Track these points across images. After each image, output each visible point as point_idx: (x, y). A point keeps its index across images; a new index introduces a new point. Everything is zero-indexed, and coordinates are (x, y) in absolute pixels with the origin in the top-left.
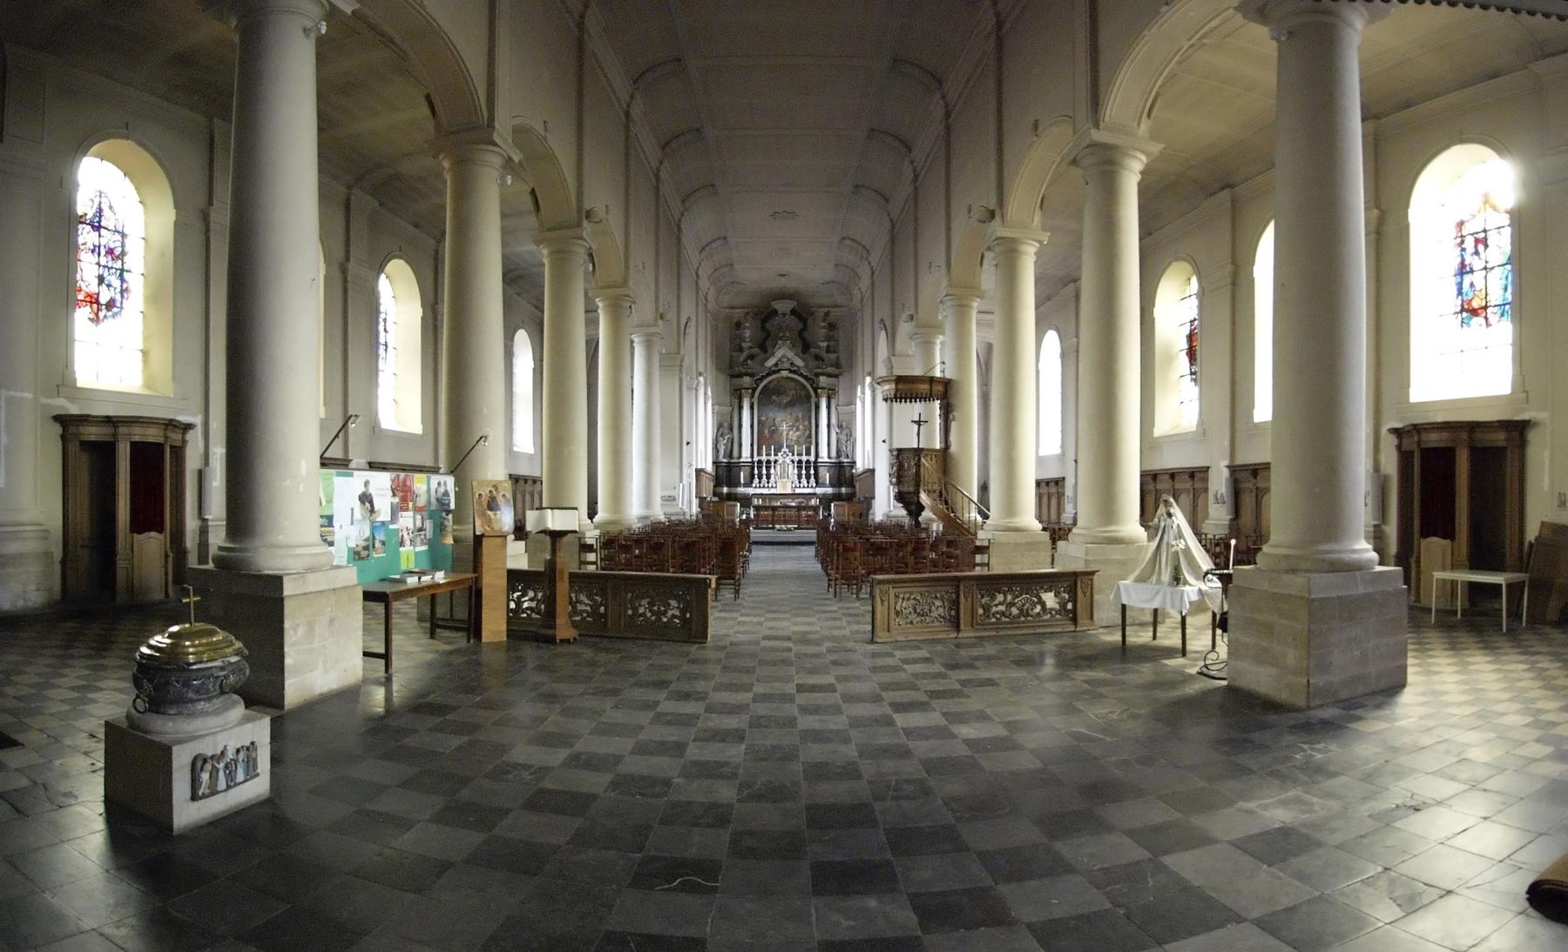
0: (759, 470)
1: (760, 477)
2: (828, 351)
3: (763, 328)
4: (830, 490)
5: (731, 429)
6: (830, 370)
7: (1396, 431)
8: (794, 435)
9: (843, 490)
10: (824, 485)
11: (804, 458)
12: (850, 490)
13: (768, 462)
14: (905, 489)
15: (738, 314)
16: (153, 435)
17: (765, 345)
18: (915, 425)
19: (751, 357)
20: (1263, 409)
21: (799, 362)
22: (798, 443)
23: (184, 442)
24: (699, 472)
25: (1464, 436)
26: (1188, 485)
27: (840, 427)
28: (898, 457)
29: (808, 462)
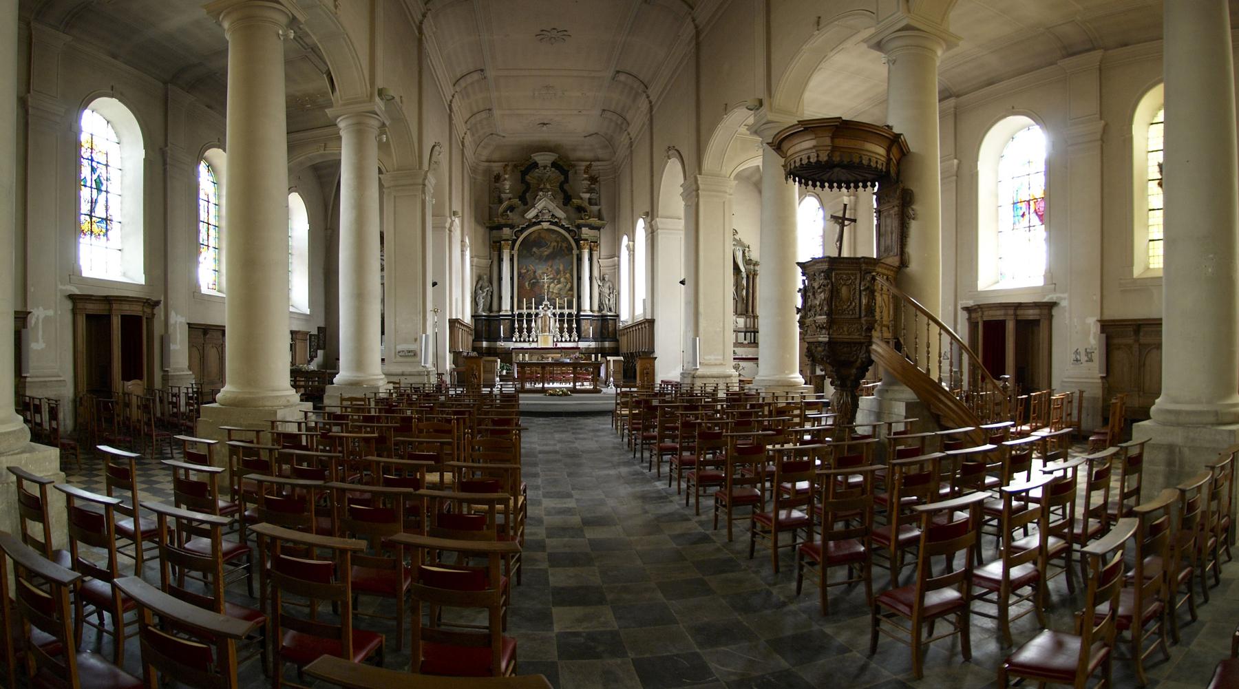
0: (520, 324)
1: (521, 331)
2: (590, 203)
3: (523, 181)
4: (593, 345)
5: (491, 282)
7: (967, 309)
8: (555, 288)
9: (607, 344)
10: (586, 339)
11: (566, 311)
13: (529, 315)
15: (497, 167)
16: (136, 310)
17: (526, 196)
19: (511, 208)
20: (1151, 252)
21: (560, 214)
22: (559, 295)
23: (153, 315)
24: (454, 323)
25: (1011, 312)
27: (603, 279)
29: (570, 315)
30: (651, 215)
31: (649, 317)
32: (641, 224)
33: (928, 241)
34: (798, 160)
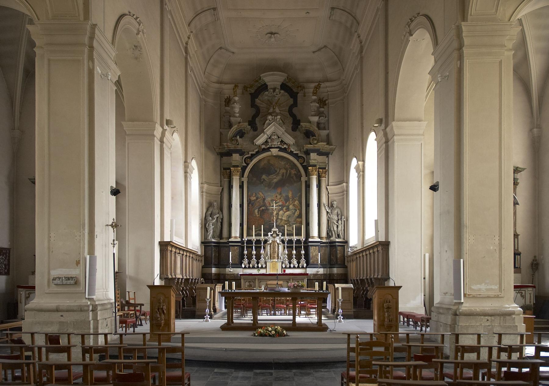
4: (321, 271)
6: (322, 145)
10: (315, 266)
27: (331, 206)
30: (385, 122)
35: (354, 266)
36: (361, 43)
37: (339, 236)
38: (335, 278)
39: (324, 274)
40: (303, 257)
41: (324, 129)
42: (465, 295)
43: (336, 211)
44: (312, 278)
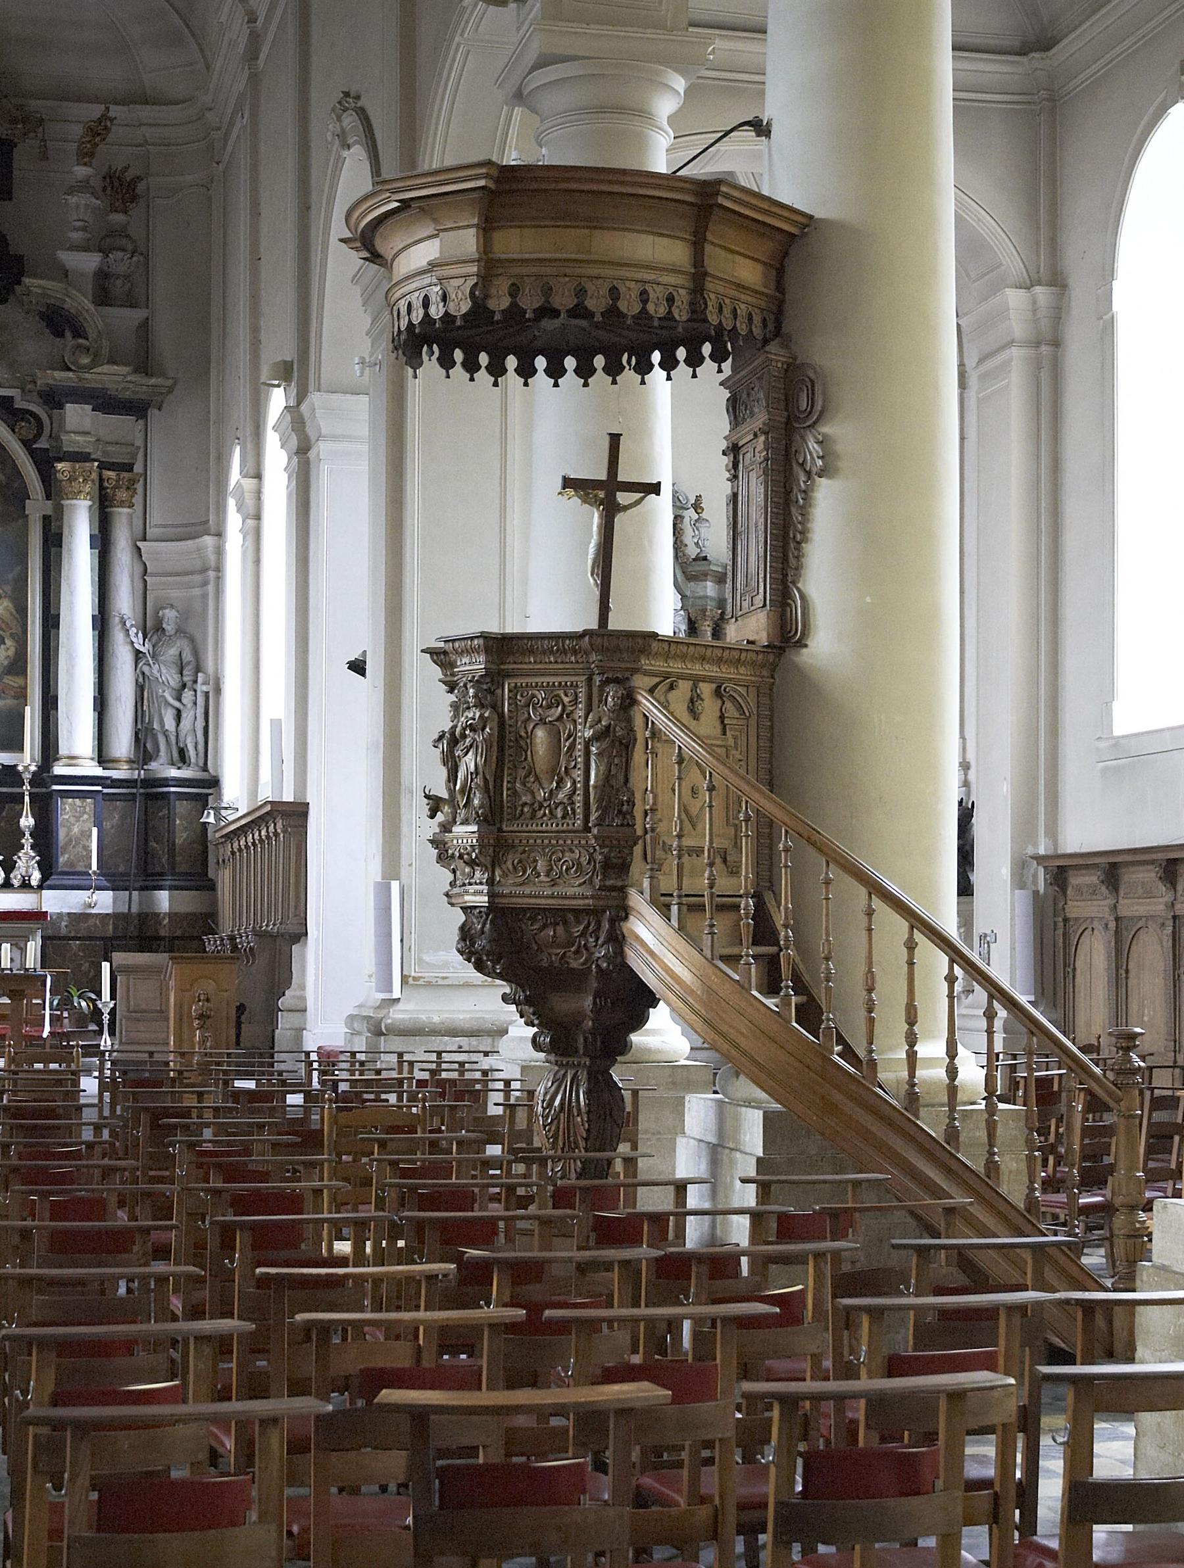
2: (103, 298)
4: (104, 901)
6: (111, 376)
9: (163, 900)
10: (76, 880)
12: (189, 901)
14: (535, 889)
18: (563, 504)
26: (1157, 905)
27: (152, 628)
28: (488, 687)
30: (296, 372)
31: (288, 797)
32: (278, 400)
33: (892, 553)
34: (416, 299)
35: (227, 881)
36: (252, 20)
37: (182, 758)
38: (163, 933)
39: (116, 916)
40: (27, 841)
41: (131, 303)
42: (404, 979)
43: (173, 652)
44: (64, 931)
